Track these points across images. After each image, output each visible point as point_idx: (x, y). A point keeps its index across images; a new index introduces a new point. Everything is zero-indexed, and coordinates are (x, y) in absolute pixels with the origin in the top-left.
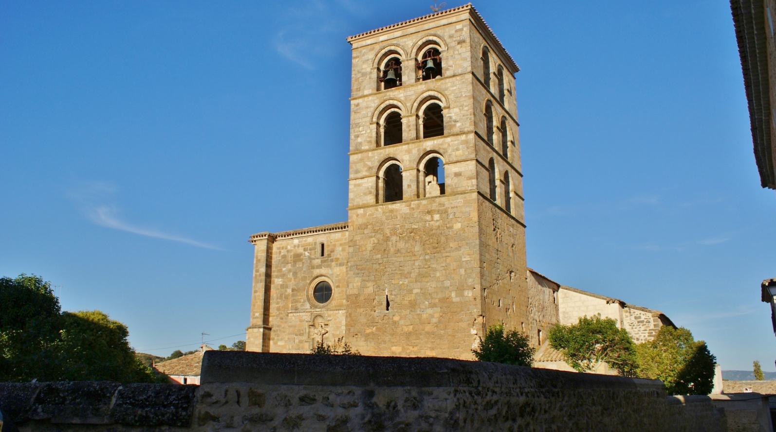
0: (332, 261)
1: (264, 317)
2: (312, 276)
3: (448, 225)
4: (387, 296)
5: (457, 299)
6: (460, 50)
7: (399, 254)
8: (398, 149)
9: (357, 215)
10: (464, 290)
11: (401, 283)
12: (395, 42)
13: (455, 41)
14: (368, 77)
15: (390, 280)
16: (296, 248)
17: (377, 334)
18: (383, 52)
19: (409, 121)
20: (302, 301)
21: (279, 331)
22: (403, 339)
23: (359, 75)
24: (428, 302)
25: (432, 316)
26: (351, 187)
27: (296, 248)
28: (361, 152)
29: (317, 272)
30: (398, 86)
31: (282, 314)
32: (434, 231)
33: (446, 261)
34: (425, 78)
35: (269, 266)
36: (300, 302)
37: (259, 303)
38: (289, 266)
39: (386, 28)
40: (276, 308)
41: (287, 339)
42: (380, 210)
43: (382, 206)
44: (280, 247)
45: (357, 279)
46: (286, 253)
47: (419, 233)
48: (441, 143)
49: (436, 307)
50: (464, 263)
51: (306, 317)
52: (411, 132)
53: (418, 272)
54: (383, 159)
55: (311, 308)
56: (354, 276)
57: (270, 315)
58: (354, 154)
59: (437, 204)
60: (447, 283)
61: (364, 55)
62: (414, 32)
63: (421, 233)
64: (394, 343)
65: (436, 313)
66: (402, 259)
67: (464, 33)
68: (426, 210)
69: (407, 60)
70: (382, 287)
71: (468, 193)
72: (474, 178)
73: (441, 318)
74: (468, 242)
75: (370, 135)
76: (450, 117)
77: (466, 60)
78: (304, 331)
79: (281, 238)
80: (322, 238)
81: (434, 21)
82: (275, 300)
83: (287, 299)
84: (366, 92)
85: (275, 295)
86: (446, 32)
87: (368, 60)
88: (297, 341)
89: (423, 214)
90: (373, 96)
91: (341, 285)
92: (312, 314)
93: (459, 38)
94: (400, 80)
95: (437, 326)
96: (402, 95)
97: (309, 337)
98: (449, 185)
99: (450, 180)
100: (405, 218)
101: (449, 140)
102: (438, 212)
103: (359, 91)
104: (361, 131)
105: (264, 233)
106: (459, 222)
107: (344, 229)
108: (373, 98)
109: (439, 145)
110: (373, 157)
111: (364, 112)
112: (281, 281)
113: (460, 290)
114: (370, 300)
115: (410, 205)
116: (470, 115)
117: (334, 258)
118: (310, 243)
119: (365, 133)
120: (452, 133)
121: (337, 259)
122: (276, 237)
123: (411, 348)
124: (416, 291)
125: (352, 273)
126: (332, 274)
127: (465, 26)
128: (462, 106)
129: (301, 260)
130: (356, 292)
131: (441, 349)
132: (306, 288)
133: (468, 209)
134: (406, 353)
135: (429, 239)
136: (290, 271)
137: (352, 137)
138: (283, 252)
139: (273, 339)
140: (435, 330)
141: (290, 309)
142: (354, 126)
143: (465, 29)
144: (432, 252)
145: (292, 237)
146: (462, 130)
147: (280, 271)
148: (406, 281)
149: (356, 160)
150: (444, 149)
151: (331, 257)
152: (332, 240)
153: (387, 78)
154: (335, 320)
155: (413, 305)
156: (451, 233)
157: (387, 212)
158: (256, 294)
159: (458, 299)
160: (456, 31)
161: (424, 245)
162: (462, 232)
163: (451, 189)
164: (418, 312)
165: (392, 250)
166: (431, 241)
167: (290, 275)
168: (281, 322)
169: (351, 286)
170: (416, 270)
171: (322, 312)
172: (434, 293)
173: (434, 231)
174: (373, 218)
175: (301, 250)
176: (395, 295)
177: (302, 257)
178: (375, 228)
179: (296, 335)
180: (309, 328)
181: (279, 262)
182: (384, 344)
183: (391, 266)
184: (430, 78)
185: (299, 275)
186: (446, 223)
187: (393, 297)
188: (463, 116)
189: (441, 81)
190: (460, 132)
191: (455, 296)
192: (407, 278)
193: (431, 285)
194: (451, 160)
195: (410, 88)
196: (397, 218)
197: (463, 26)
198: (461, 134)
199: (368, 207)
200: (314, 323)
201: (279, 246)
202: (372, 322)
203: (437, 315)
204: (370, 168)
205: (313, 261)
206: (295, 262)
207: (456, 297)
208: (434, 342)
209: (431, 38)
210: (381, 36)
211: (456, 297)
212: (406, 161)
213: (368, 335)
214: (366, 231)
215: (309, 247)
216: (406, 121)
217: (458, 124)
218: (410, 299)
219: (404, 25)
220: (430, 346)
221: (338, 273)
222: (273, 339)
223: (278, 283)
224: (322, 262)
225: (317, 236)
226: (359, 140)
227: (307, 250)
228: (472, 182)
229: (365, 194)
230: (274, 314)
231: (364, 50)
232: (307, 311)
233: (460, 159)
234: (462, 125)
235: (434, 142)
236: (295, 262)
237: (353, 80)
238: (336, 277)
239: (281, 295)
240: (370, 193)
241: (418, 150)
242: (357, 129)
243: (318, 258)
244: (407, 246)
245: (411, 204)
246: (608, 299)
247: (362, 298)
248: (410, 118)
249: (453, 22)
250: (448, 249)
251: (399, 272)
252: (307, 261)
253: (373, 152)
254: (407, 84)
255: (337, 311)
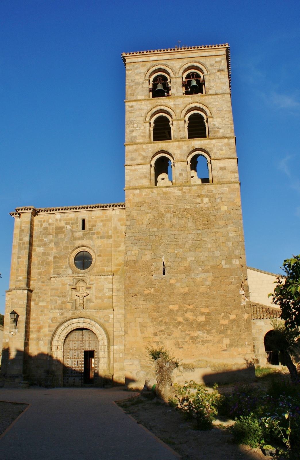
0: (93, 234)
1: (27, 280)
2: (74, 246)
3: (216, 207)
4: (164, 262)
5: (227, 266)
6: (219, 76)
7: (173, 229)
8: (170, 145)
9: (134, 195)
10: (232, 259)
11: (176, 252)
12: (164, 62)
13: (215, 69)
14: (141, 86)
15: (167, 250)
16: (58, 222)
17: (156, 295)
18: (154, 69)
19: (178, 124)
20: (64, 267)
21: (40, 293)
22: (180, 299)
23: (133, 84)
24: (201, 268)
25: (206, 280)
26: (126, 171)
27: (58, 222)
28: (136, 144)
29: (78, 243)
30: (166, 96)
31: (43, 278)
32: (204, 212)
33: (215, 235)
34: (187, 93)
35: (31, 236)
36: (62, 268)
37: (22, 268)
38: (51, 237)
39: (157, 51)
40: (37, 273)
41: (49, 300)
42: (155, 192)
43: (156, 189)
44: (42, 220)
45: (135, 248)
46: (48, 226)
47: (191, 212)
48: (207, 143)
49: (208, 272)
50: (231, 238)
51: (69, 281)
52: (180, 132)
53: (191, 243)
54: (156, 151)
55: (73, 273)
56: (132, 245)
57: (31, 278)
58: (129, 145)
59: (206, 190)
60: (217, 253)
61: (136, 69)
62: (180, 57)
63: (192, 212)
64: (170, 302)
65: (209, 277)
66: (176, 232)
67: (222, 64)
68: (197, 195)
69: (176, 78)
70: (159, 255)
71: (232, 183)
72: (237, 173)
73: (213, 281)
74: (234, 221)
75: (144, 131)
76: (214, 125)
77: (226, 84)
78: (67, 293)
79: (43, 212)
80: (83, 214)
81: (197, 52)
82: (36, 266)
83: (49, 265)
84: (139, 98)
85: (36, 262)
86: (208, 62)
87: (140, 73)
88: (59, 302)
89: (194, 197)
90: (146, 101)
91: (102, 254)
92: (74, 278)
93: (218, 68)
94: (168, 93)
95: (210, 288)
96: (172, 103)
97: (71, 299)
98: (215, 176)
99: (217, 172)
100: (178, 200)
101: (214, 141)
102: (207, 196)
103: (133, 96)
104: (135, 128)
105: (29, 207)
106: (225, 206)
107: (105, 208)
108: (146, 103)
109: (205, 144)
110: (148, 149)
111: (138, 113)
112: (43, 249)
113: (229, 259)
114: (147, 266)
115: (182, 190)
116: (231, 125)
117: (95, 231)
118: (71, 218)
119: (139, 130)
120: (216, 137)
121: (98, 233)
122: (39, 212)
123: (187, 306)
124: (189, 259)
125: (130, 242)
126: (93, 245)
127: (224, 60)
128: (224, 117)
129: (63, 232)
130: (134, 258)
131: (215, 307)
132: (68, 256)
133: (232, 196)
134: (183, 310)
135: (200, 217)
136: (51, 241)
137: (127, 131)
138: (45, 225)
139: (34, 300)
140: (209, 291)
141: (52, 274)
142: (129, 122)
143: (223, 61)
144: (203, 228)
145: (54, 212)
146: (224, 135)
147: (42, 240)
148: (181, 251)
149: (131, 150)
150: (210, 148)
151: (92, 231)
152: (93, 217)
153: (157, 89)
154: (98, 284)
155: (188, 271)
156: (218, 214)
157: (161, 194)
158: (20, 260)
159: (227, 266)
160: (216, 62)
161: (195, 222)
162: (228, 213)
163: (217, 179)
164: (193, 276)
165: (167, 225)
166: (202, 219)
167: (52, 245)
168: (43, 285)
169: (129, 253)
170: (189, 242)
171: (85, 277)
172: (206, 261)
173: (204, 212)
174: (149, 198)
175: (63, 224)
176: (171, 262)
177: (64, 230)
178: (150, 206)
179: (58, 297)
180: (72, 291)
181: (41, 233)
182: (162, 303)
183: (166, 238)
184: (193, 94)
185: (61, 245)
186: (214, 205)
187: (169, 263)
188: (225, 125)
189: (205, 97)
190: (223, 136)
191: (224, 264)
192: (182, 248)
193: (203, 255)
194: (216, 157)
195: (179, 99)
196: (170, 199)
197: (221, 59)
198: (224, 138)
199: (144, 188)
200: (76, 287)
201: (40, 219)
202: (151, 285)
203: (210, 279)
204: (145, 158)
205: (75, 233)
206: (57, 234)
207: (226, 264)
208: (208, 301)
209: (195, 64)
210: (151, 56)
211: (226, 264)
212: (178, 154)
213: (147, 295)
214: (142, 208)
215: (70, 222)
216: (176, 124)
217: (221, 131)
218: (185, 265)
219: (172, 51)
220: (204, 304)
221: (100, 245)
222: (34, 300)
223: (39, 251)
224: (83, 234)
225: (79, 213)
226: (134, 134)
227: (69, 224)
228: (235, 176)
229: (141, 178)
230: (35, 278)
231: (137, 65)
232: (70, 276)
233: (224, 157)
234: (225, 131)
235: (201, 143)
236: (57, 234)
237: (127, 87)
238: (98, 248)
239: (43, 262)
240: (146, 177)
241: (188, 147)
242: (131, 126)
243: (79, 231)
244: (180, 222)
245: (183, 188)
246: (278, 276)
247: (140, 264)
248: (180, 122)
249: (213, 55)
250: (217, 226)
251: (174, 243)
252: (68, 233)
253: (147, 145)
254: (175, 95)
255: (99, 277)
